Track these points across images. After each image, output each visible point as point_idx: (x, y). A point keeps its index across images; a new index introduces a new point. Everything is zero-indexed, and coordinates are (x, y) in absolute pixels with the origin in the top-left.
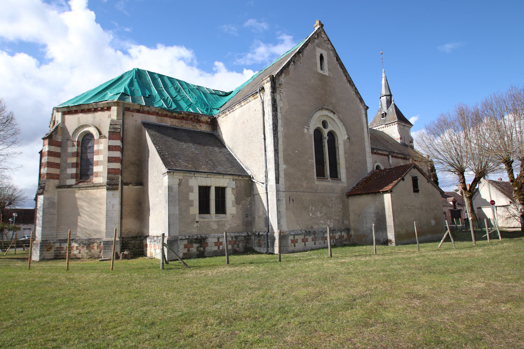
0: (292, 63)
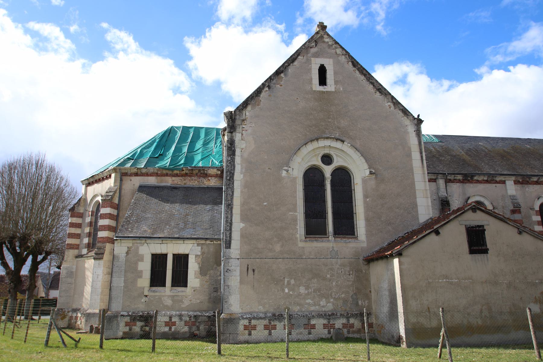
0: (267, 89)
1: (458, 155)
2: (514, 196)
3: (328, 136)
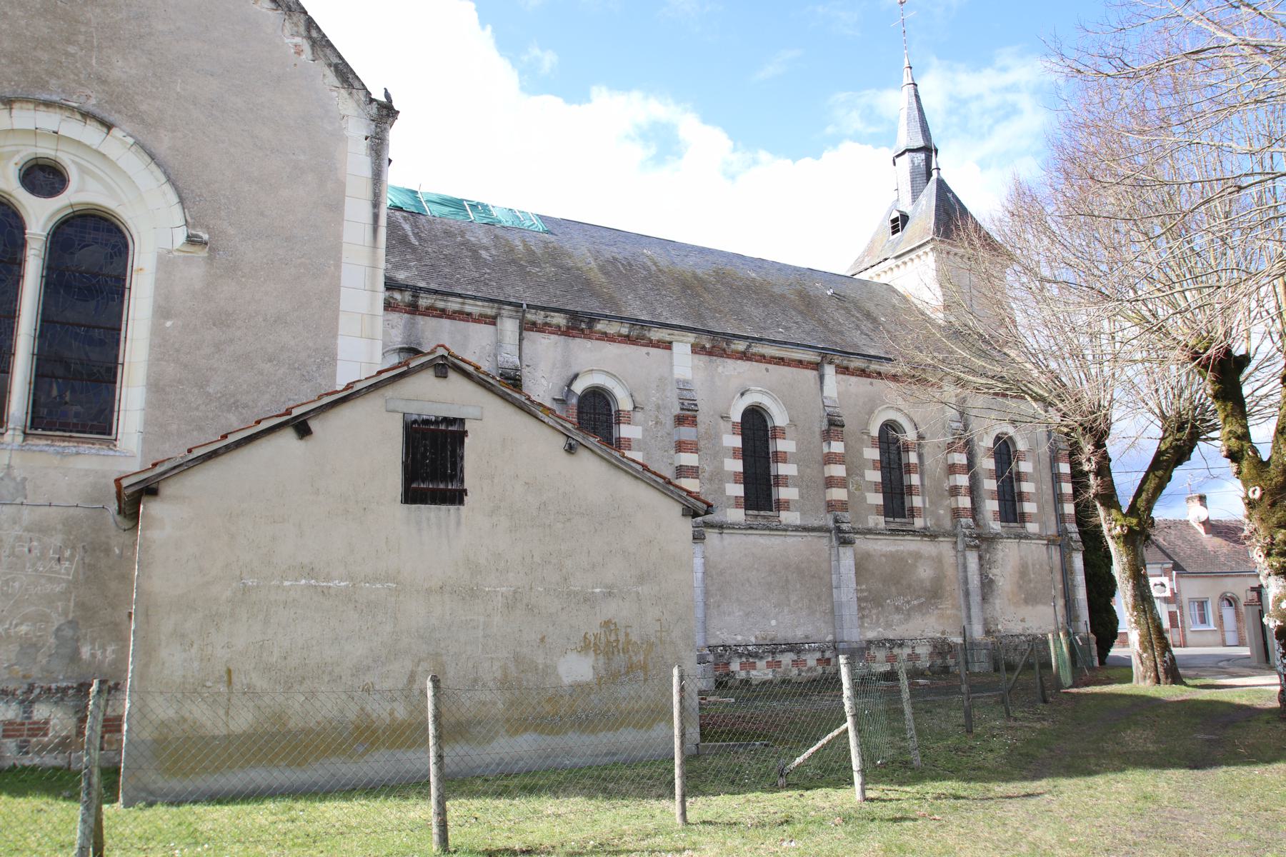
1: (578, 269)
2: (686, 382)
3: (55, 98)
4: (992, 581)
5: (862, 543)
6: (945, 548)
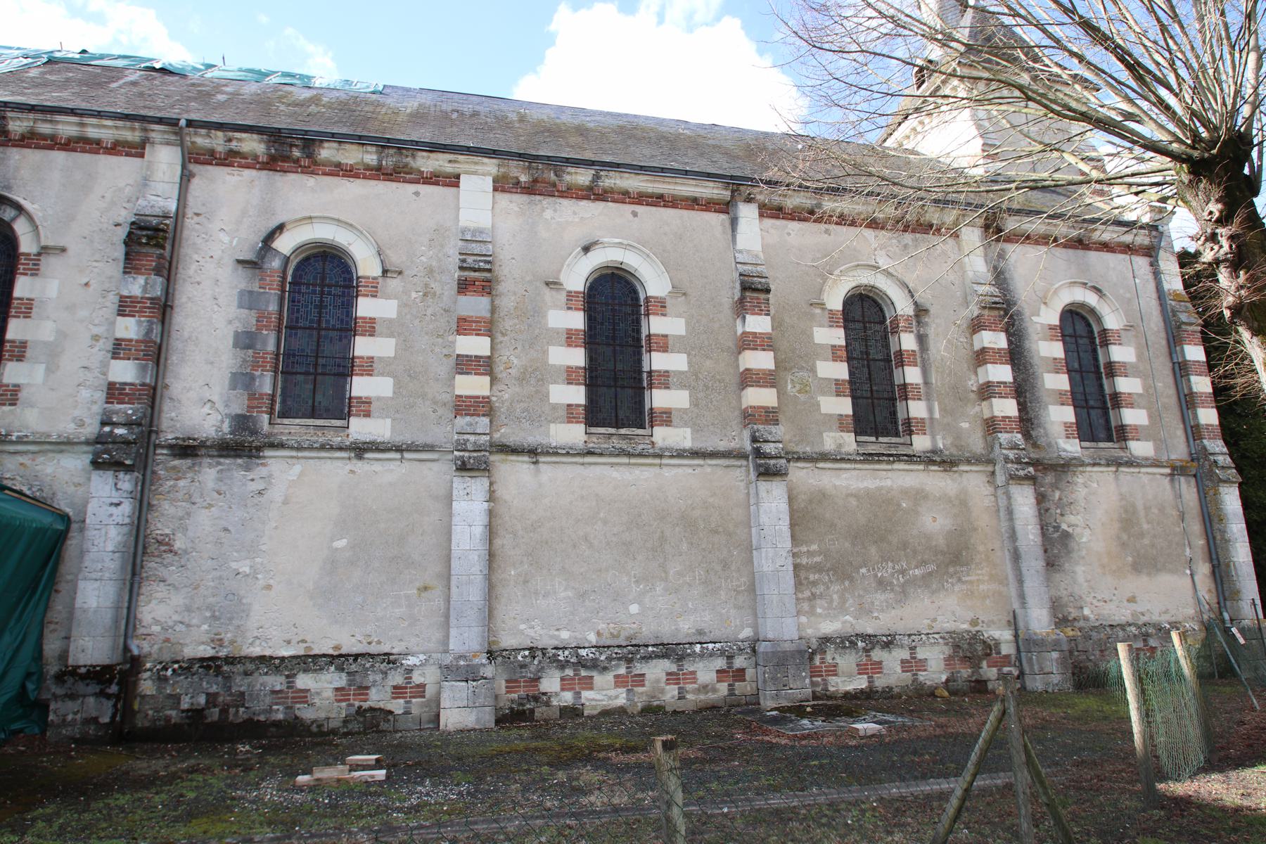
4: (1066, 535)
5: (800, 474)
6: (973, 482)
